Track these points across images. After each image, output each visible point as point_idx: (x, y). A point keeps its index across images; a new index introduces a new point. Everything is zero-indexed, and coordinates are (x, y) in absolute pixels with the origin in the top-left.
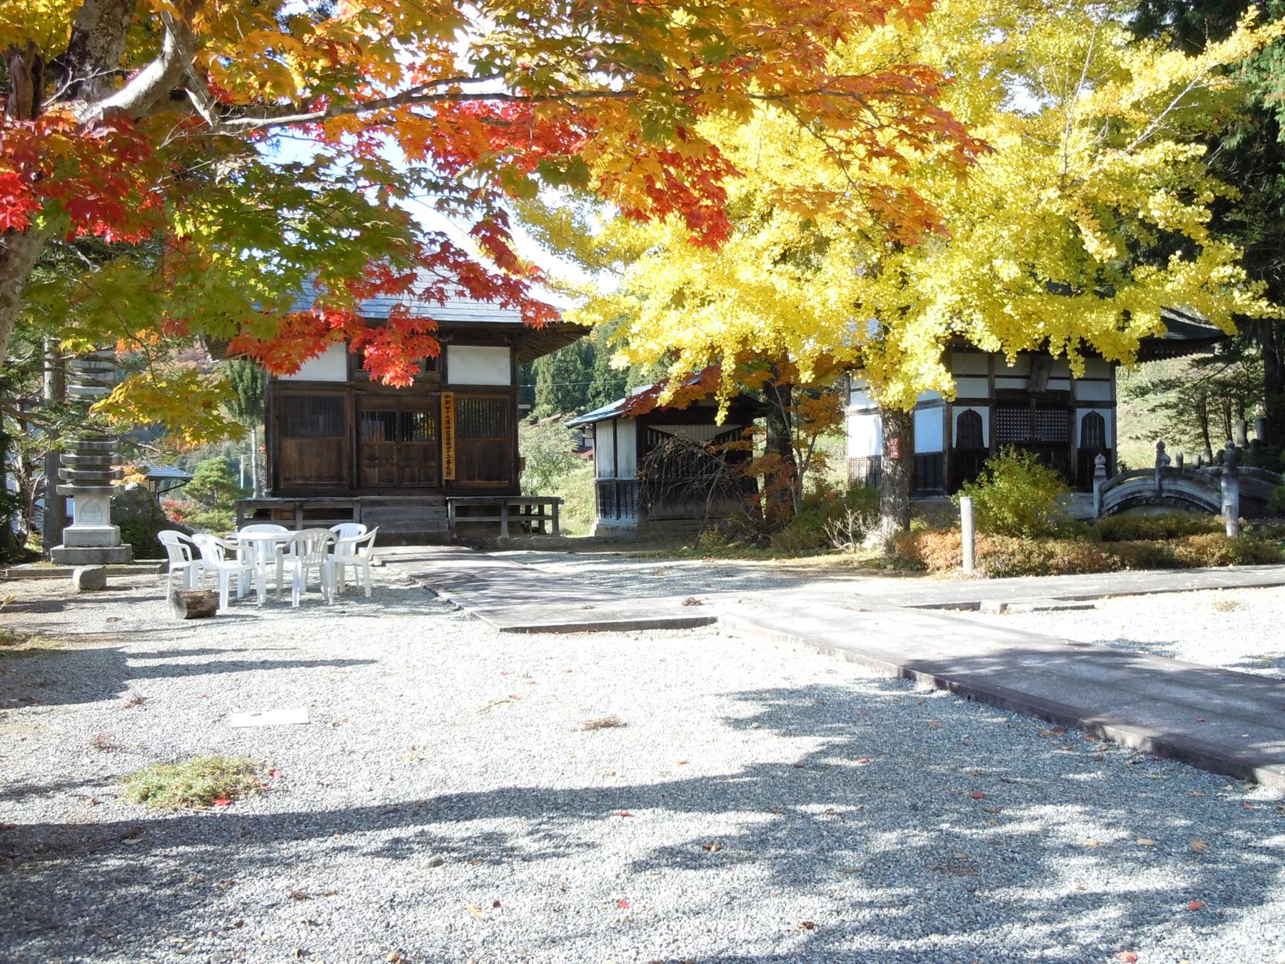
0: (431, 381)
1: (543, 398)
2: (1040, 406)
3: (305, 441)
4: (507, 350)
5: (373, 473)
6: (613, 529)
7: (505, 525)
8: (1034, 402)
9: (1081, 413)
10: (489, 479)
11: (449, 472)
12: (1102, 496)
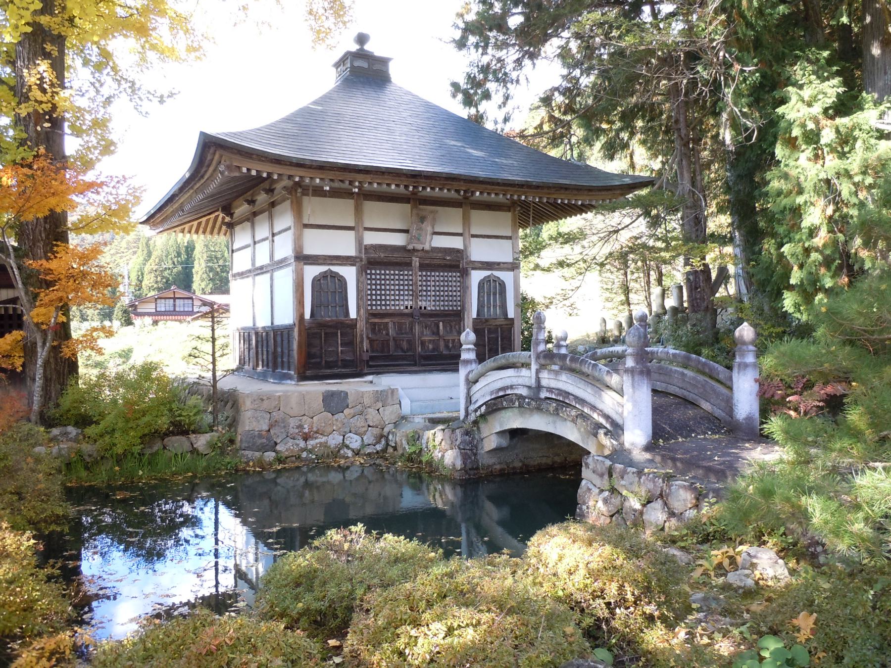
1: (199, 276)
2: (422, 267)
8: (416, 262)
9: (476, 276)
12: (469, 390)
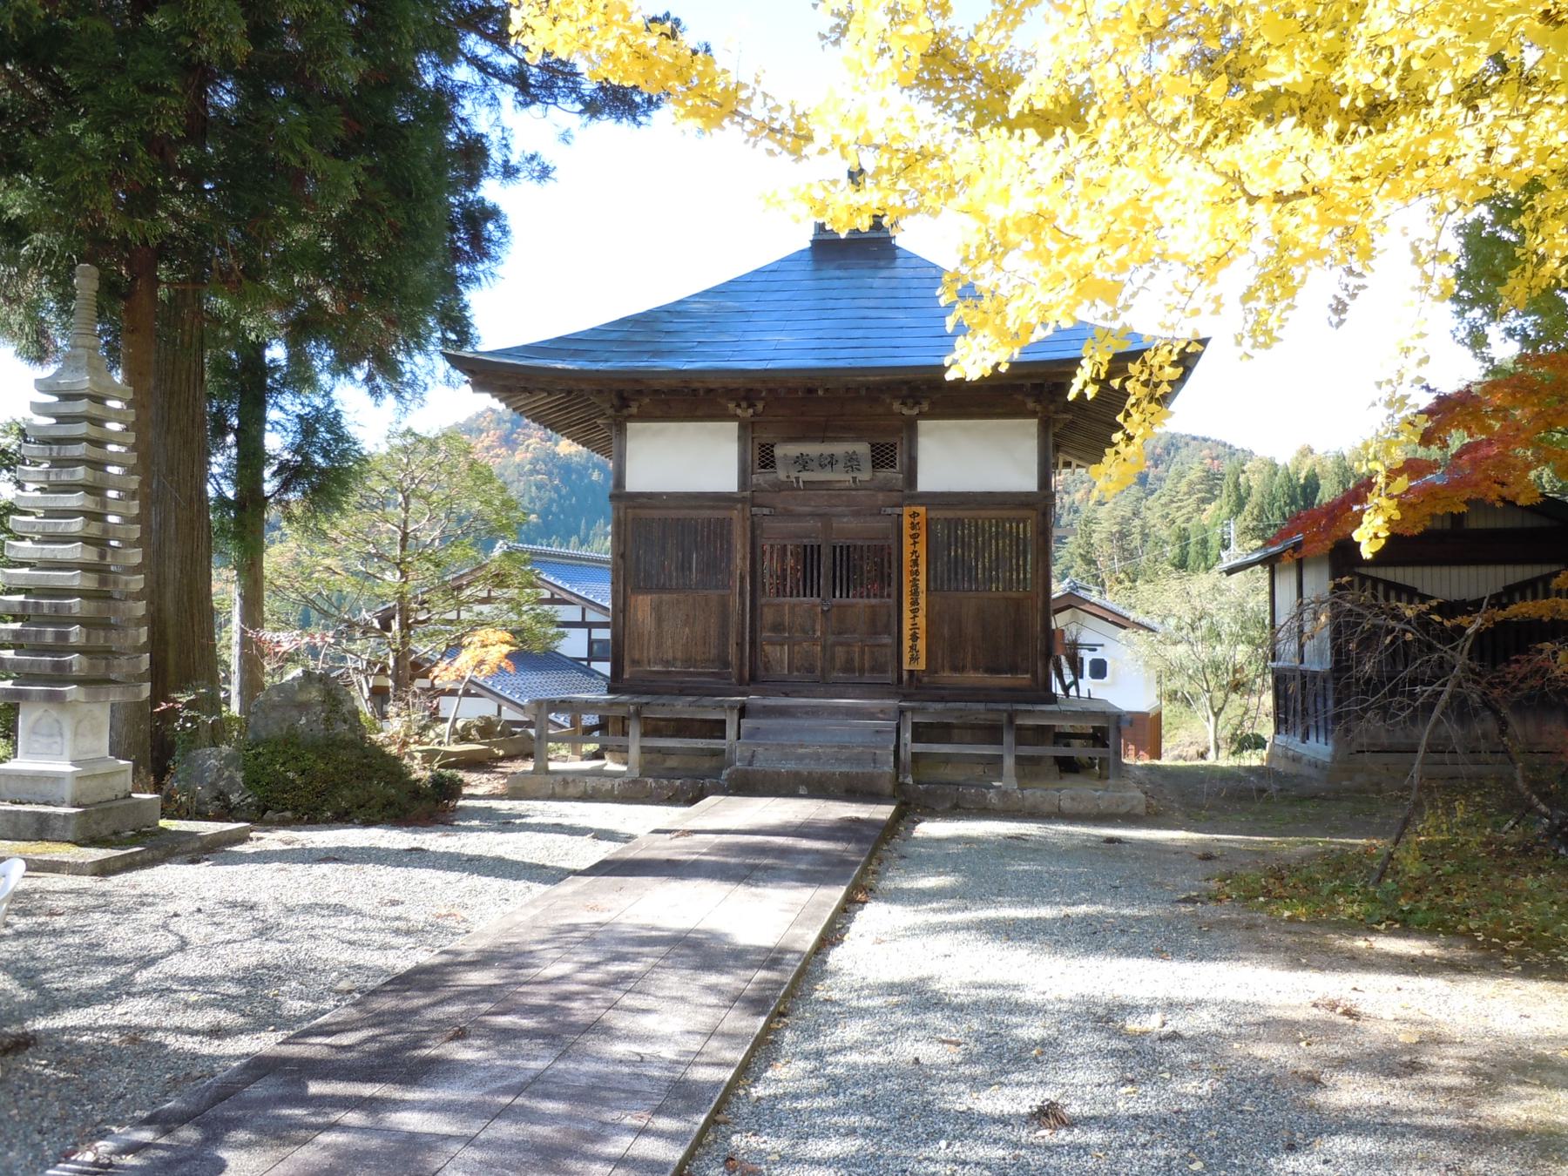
0: (886, 488)
3: (666, 597)
4: (1032, 425)
5: (778, 655)
6: (1296, 759)
7: (1009, 763)
10: (993, 670)
11: (915, 656)
